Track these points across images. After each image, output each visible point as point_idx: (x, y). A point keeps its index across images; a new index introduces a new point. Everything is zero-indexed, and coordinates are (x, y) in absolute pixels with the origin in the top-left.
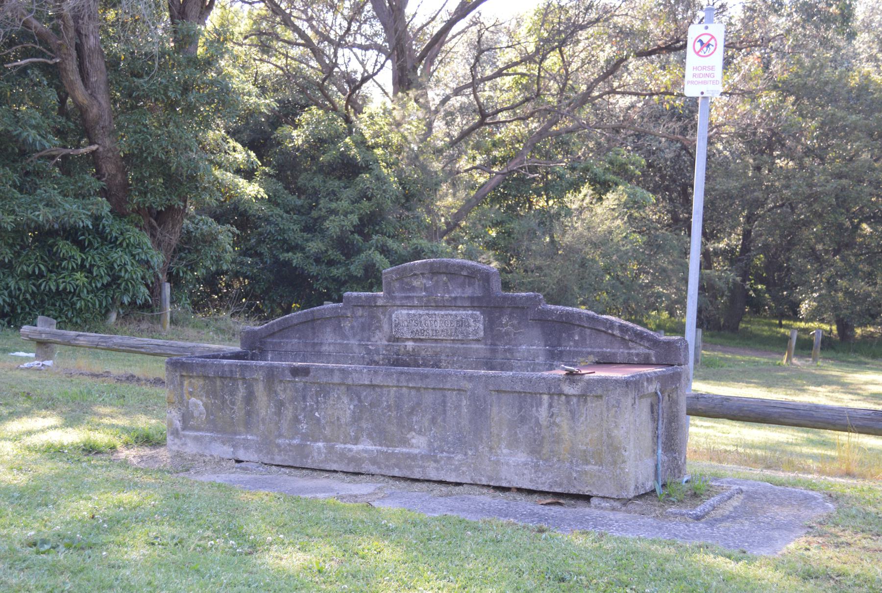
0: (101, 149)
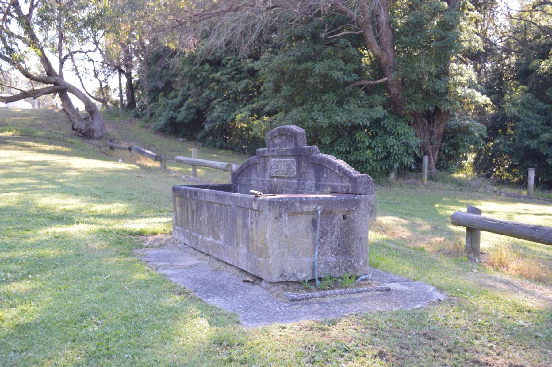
0: (389, 80)
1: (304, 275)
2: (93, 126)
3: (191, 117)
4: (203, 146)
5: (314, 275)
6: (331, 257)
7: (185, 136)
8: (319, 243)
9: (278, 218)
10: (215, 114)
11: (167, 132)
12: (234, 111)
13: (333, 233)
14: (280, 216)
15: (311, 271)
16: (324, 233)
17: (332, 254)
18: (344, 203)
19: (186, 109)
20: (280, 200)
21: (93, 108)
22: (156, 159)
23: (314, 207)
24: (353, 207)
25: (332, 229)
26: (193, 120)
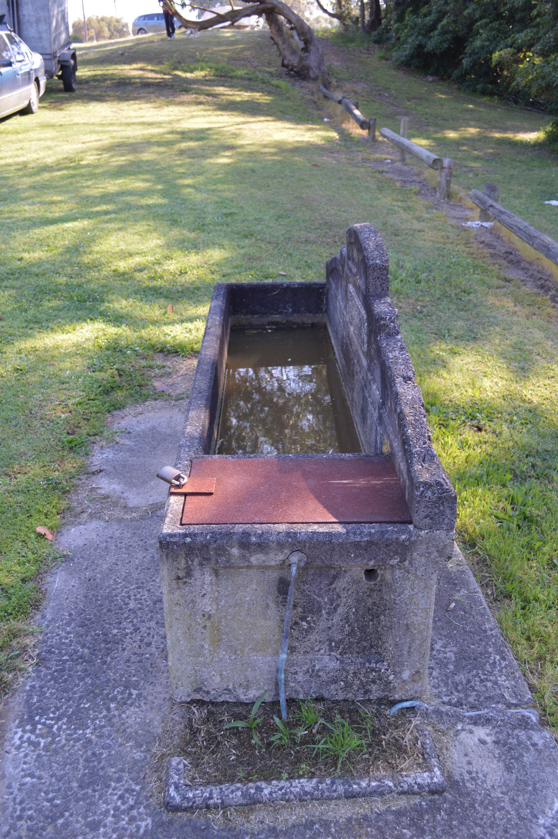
1: (252, 693)
2: (308, 62)
3: (445, 45)
4: (459, 89)
5: (277, 694)
6: (326, 658)
7: (436, 73)
8: (293, 632)
9: (183, 578)
10: (478, 43)
11: (413, 67)
12: (506, 38)
13: (335, 609)
14: (189, 573)
15: (272, 687)
16: (311, 609)
17: (331, 649)
18: (367, 548)
19: (440, 34)
20: (188, 540)
21: (308, 36)
22: (363, 125)
23: (281, 557)
24: (392, 558)
25: (331, 601)
26: (449, 49)
